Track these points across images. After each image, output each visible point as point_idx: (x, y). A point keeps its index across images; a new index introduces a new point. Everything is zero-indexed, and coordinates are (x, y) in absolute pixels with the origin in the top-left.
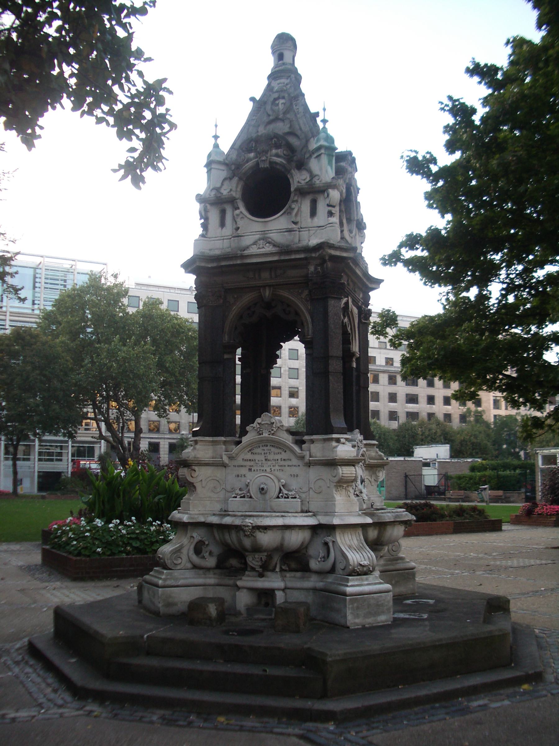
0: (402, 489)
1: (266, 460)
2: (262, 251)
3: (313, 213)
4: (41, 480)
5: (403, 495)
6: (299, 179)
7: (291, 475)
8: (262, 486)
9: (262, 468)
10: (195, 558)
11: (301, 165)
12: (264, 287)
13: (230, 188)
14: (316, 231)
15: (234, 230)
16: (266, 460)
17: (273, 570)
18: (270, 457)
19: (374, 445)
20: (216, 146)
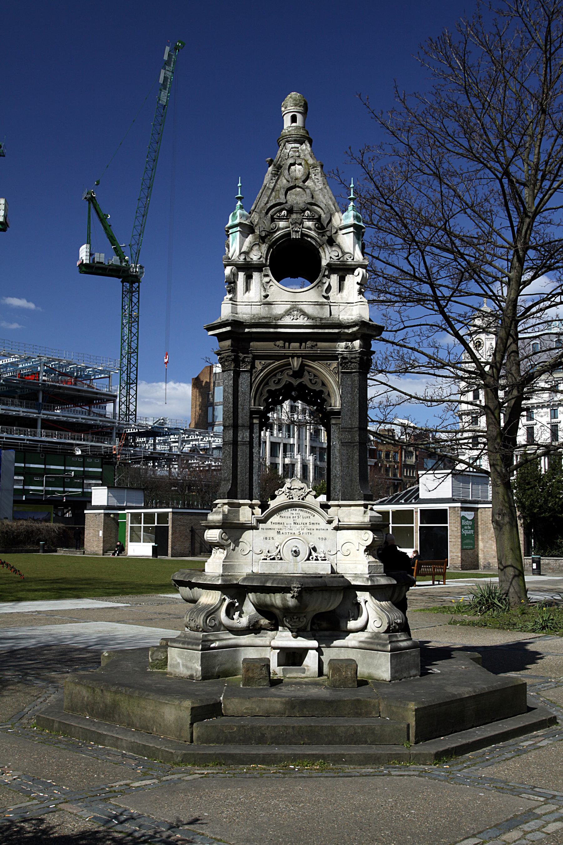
0: (188, 544)
1: (295, 523)
2: (295, 322)
4: (425, 522)
6: (327, 256)
7: (319, 538)
8: (294, 549)
9: (291, 531)
12: (293, 357)
13: (260, 254)
14: (346, 306)
15: (262, 297)
16: (295, 523)
18: (299, 521)
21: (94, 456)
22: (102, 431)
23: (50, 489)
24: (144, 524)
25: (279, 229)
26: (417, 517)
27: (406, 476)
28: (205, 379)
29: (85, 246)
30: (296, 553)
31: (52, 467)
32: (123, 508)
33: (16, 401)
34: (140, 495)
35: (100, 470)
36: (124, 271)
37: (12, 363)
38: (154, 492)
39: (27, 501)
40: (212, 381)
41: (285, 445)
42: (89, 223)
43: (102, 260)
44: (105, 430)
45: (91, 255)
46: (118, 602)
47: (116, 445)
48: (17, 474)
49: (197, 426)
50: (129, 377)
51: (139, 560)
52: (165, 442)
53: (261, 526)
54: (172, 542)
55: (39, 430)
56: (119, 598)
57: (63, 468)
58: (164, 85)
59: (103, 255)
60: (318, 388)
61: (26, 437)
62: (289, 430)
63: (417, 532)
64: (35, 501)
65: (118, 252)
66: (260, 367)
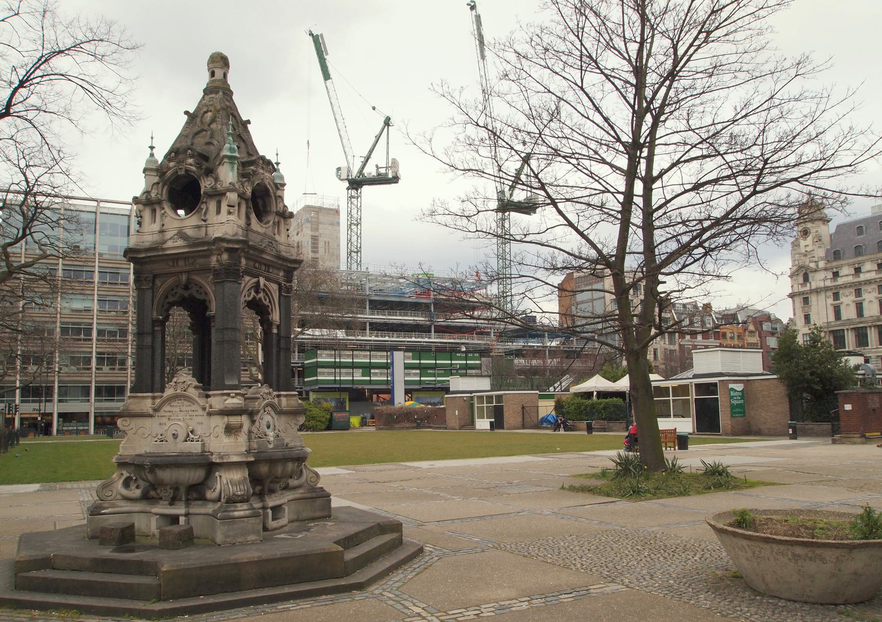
0: (520, 419)
2: (176, 244)
3: (218, 212)
5: (520, 424)
6: (206, 184)
10: (124, 492)
11: (210, 172)
12: (181, 273)
17: (180, 500)
18: (184, 409)
19: (295, 395)
20: (152, 155)
25: (170, 169)
26: (693, 390)
30: (175, 436)
51: (482, 432)
53: (157, 414)
60: (201, 297)
66: (159, 284)
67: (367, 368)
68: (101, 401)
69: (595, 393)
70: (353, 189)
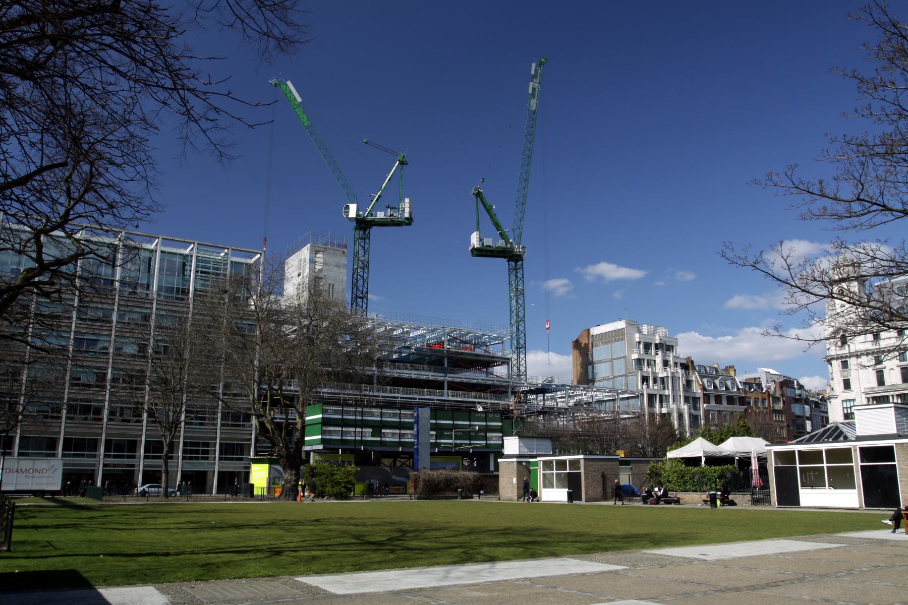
0: (600, 489)
5: (600, 496)
21: (495, 412)
22: (498, 390)
23: (459, 442)
24: (828, 462)
27: (776, 421)
28: (584, 341)
29: (475, 233)
31: (460, 422)
32: (535, 456)
33: (426, 366)
34: (548, 444)
35: (500, 424)
36: (509, 252)
37: (421, 336)
38: (560, 442)
39: (440, 453)
40: (590, 342)
41: (661, 396)
42: (478, 213)
43: (490, 244)
44: (501, 389)
45: (481, 240)
46: (608, 562)
47: (511, 401)
48: (432, 429)
49: (579, 382)
50: (518, 343)
51: (554, 506)
52: (552, 398)
54: (586, 487)
55: (446, 391)
56: (610, 555)
57: (468, 423)
58: (533, 95)
59: (490, 240)
61: (435, 398)
62: (663, 383)
63: (857, 472)
64: (446, 453)
65: (502, 235)
67: (378, 427)
68: (69, 456)
69: (703, 460)
70: (361, 229)
